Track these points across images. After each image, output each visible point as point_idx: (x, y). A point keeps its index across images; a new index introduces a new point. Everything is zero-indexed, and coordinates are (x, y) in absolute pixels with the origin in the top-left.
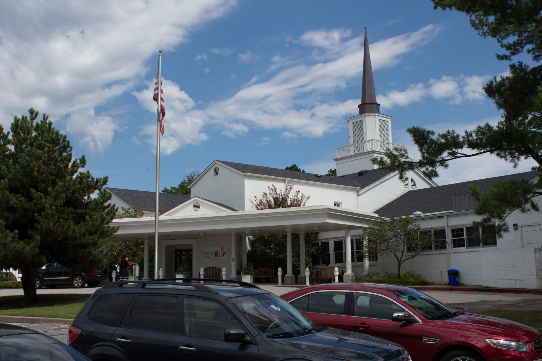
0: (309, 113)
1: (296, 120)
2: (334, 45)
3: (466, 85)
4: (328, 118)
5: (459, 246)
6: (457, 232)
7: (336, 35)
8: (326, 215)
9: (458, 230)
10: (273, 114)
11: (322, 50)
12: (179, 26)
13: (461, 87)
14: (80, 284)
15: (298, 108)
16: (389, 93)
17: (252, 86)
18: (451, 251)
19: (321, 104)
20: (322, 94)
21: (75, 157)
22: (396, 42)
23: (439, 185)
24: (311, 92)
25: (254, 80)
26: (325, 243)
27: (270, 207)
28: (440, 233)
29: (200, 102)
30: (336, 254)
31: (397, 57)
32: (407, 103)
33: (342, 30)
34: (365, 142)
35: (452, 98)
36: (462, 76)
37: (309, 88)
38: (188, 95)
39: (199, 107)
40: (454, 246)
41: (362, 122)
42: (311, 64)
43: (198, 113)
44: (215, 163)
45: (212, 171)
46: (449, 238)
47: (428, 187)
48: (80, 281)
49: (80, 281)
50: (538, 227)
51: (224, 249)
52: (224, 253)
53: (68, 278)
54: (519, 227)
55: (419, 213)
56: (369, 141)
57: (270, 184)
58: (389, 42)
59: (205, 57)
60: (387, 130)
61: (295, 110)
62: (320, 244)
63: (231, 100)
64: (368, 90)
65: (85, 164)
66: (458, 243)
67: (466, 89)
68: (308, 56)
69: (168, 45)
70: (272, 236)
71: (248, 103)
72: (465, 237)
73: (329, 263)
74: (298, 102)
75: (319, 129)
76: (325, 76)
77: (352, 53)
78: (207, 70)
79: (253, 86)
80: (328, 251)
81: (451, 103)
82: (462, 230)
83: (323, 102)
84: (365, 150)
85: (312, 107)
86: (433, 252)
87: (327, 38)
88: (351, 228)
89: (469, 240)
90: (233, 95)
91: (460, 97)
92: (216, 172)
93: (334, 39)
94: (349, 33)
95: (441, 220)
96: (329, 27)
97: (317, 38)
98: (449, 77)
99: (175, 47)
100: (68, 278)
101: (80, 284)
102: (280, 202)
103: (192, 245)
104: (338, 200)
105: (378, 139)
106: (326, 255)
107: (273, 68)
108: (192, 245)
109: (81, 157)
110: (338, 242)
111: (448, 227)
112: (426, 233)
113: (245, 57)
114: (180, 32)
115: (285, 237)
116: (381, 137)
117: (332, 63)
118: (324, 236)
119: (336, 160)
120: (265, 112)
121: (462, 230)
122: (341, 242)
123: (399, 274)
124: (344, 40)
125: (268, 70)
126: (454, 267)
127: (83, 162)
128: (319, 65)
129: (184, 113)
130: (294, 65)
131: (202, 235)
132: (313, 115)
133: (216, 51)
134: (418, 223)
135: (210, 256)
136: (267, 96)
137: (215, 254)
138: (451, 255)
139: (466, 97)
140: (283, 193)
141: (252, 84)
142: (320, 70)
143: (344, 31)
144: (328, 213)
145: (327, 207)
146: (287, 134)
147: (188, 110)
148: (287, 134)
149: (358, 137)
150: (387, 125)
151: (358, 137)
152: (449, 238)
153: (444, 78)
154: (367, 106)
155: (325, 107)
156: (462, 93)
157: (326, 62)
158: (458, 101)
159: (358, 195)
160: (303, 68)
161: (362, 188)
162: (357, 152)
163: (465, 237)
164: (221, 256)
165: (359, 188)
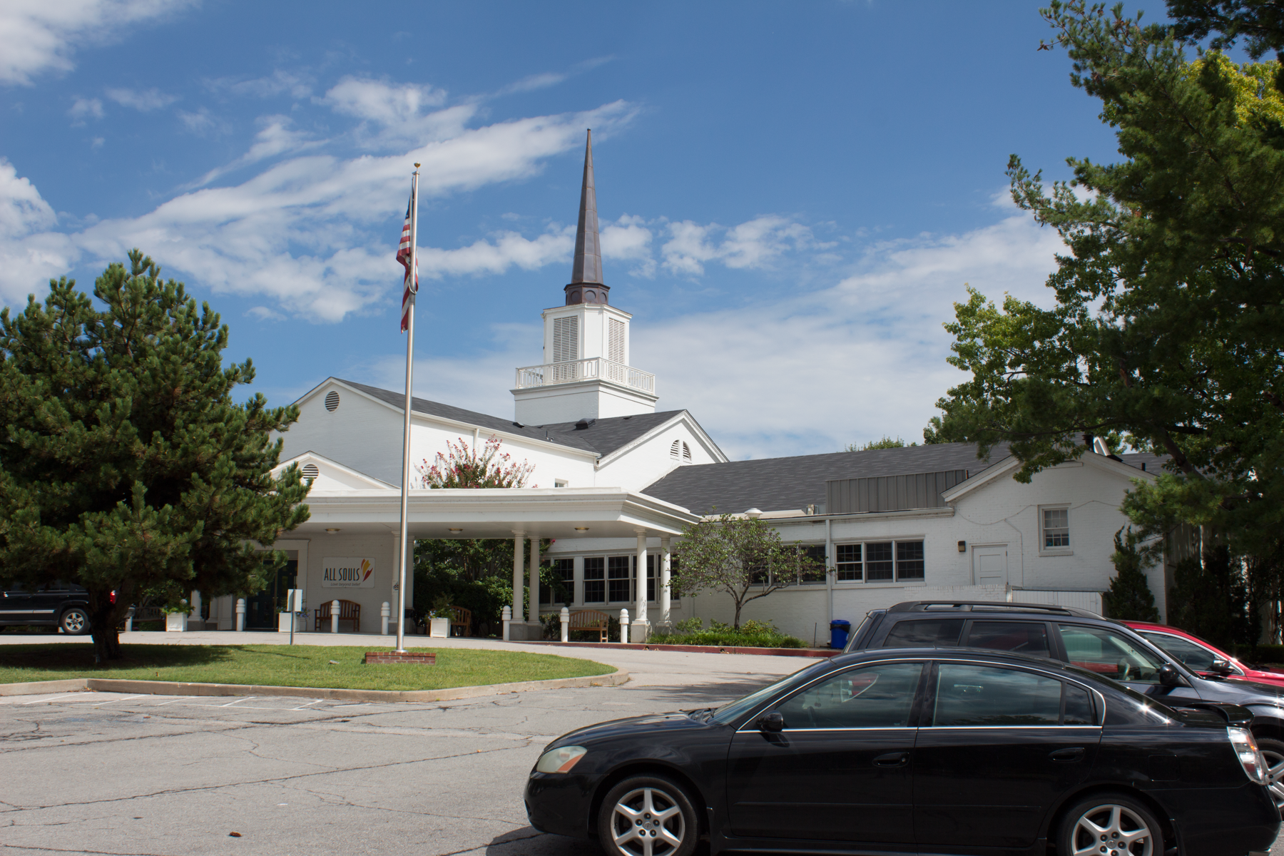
0: (319, 267)
1: (286, 280)
2: (404, 120)
3: (669, 238)
4: (363, 282)
5: (850, 577)
6: (848, 551)
7: (413, 97)
8: (620, 507)
9: (849, 548)
10: (237, 260)
11: (375, 128)
12: (48, 26)
13: (657, 244)
14: (79, 627)
15: (297, 251)
16: (503, 237)
17: (201, 192)
18: (835, 587)
19: (350, 249)
20: (357, 225)
21: (228, 359)
22: (539, 129)
23: (732, 460)
24: (340, 219)
25: (211, 176)
26: (564, 561)
27: (450, 484)
28: (817, 552)
29: (64, 214)
30: (588, 585)
31: (539, 161)
32: (540, 264)
33: (428, 88)
34: (583, 361)
35: (637, 264)
36: (663, 218)
37: (333, 210)
38: (40, 190)
39: (62, 228)
40: (841, 577)
41: (574, 320)
42: (347, 154)
43: (59, 240)
44: (331, 384)
45: (321, 400)
46: (831, 561)
47: (712, 462)
48: (80, 619)
49: (80, 619)
50: (1003, 550)
51: (368, 564)
52: (368, 573)
53: (51, 611)
54: (968, 547)
55: (756, 511)
56: (590, 360)
57: (454, 437)
58: (525, 125)
59: (97, 108)
60: (622, 340)
61: (288, 255)
62: (552, 564)
63: (147, 220)
64: (588, 255)
65: (252, 377)
66: (849, 573)
67: (667, 248)
68: (340, 135)
69: (14, 69)
70: (459, 541)
71: (175, 226)
72: (863, 560)
73: (572, 600)
74: (305, 238)
75: (336, 306)
76: (376, 186)
77: (442, 141)
78: (99, 141)
79: (206, 191)
80: (571, 575)
81: (633, 274)
82: (858, 548)
83: (355, 244)
84: (580, 379)
85: (330, 253)
86: (798, 587)
87: (391, 101)
88: (650, 533)
89: (870, 566)
90: (151, 208)
91: (653, 263)
92: (332, 402)
93: (407, 108)
94: (443, 94)
95: (818, 527)
96: (399, 77)
97: (368, 97)
98: (636, 218)
99: (32, 77)
100: (51, 611)
101: (79, 627)
102: (468, 475)
103: (296, 552)
104: (562, 478)
105: (606, 356)
106: (565, 584)
107: (258, 152)
108: (296, 552)
109: (244, 361)
110: (594, 560)
111: (831, 541)
112: (789, 550)
113: (196, 121)
114: (48, 40)
115: (511, 544)
116: (610, 353)
117: (394, 158)
118: (562, 548)
119: (515, 392)
120: (219, 253)
121: (858, 548)
122: (626, 559)
123: (736, 626)
124: (426, 110)
125: (247, 157)
126: (840, 615)
127: (248, 372)
128: (364, 160)
129: (19, 238)
130: (307, 154)
131: (332, 532)
132: (328, 272)
133: (124, 97)
134: (778, 530)
135: (338, 577)
136: (234, 220)
137: (348, 574)
138: (835, 594)
139: (665, 265)
140: (479, 455)
141: (203, 188)
142: (365, 170)
143: (431, 92)
144: (625, 504)
145: (623, 491)
146: (263, 312)
147: (33, 230)
148: (263, 312)
149: (565, 351)
150: (622, 332)
151: (565, 351)
152: (831, 561)
153: (624, 219)
154: (585, 289)
155: (358, 254)
156: (658, 256)
157: (383, 153)
158: (648, 271)
159: (596, 469)
160: (327, 161)
161: (603, 456)
162: (561, 381)
163: (863, 560)
164: (362, 577)
165: (599, 455)
